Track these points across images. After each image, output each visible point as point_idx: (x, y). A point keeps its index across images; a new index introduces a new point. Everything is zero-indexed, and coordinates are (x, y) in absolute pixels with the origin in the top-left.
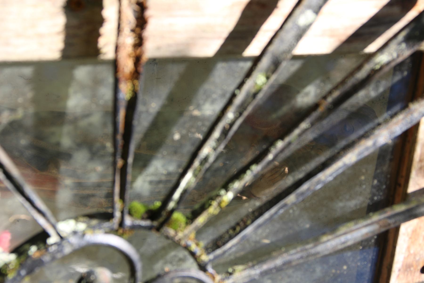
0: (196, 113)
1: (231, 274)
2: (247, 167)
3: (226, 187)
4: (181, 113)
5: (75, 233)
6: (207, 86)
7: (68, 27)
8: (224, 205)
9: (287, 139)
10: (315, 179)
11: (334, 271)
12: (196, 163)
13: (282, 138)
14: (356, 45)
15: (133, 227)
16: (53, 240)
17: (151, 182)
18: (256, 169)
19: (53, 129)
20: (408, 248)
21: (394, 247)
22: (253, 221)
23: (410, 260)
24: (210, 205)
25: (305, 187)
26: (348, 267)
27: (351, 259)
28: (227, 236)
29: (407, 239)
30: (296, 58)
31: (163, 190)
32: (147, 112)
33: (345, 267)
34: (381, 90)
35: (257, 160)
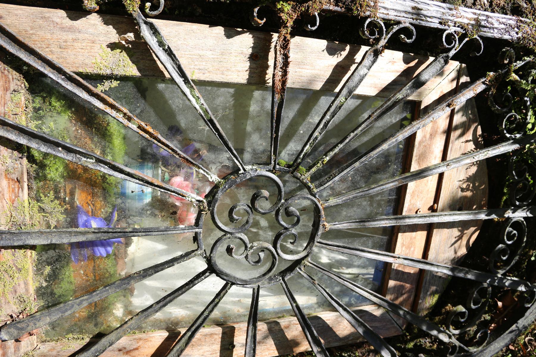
0: (311, 120)
1: (328, 200)
2: (337, 145)
3: (326, 155)
4: (304, 120)
5: (252, 169)
6: (316, 107)
7: (250, 67)
8: (324, 163)
9: (356, 132)
10: (368, 156)
11: (375, 211)
12: (311, 141)
13: (353, 132)
14: (386, 94)
15: (280, 170)
16: (242, 171)
17: (288, 154)
18: (341, 146)
19: (145, 292)
20: (410, 200)
21: (404, 200)
22: (338, 174)
23: (411, 207)
24: (318, 163)
25: (345, 282)
26: (382, 210)
27: (384, 205)
28: (326, 181)
29: (410, 196)
30: (359, 97)
31: (294, 157)
32: (288, 117)
33: (381, 209)
34: (398, 120)
35: (341, 142)
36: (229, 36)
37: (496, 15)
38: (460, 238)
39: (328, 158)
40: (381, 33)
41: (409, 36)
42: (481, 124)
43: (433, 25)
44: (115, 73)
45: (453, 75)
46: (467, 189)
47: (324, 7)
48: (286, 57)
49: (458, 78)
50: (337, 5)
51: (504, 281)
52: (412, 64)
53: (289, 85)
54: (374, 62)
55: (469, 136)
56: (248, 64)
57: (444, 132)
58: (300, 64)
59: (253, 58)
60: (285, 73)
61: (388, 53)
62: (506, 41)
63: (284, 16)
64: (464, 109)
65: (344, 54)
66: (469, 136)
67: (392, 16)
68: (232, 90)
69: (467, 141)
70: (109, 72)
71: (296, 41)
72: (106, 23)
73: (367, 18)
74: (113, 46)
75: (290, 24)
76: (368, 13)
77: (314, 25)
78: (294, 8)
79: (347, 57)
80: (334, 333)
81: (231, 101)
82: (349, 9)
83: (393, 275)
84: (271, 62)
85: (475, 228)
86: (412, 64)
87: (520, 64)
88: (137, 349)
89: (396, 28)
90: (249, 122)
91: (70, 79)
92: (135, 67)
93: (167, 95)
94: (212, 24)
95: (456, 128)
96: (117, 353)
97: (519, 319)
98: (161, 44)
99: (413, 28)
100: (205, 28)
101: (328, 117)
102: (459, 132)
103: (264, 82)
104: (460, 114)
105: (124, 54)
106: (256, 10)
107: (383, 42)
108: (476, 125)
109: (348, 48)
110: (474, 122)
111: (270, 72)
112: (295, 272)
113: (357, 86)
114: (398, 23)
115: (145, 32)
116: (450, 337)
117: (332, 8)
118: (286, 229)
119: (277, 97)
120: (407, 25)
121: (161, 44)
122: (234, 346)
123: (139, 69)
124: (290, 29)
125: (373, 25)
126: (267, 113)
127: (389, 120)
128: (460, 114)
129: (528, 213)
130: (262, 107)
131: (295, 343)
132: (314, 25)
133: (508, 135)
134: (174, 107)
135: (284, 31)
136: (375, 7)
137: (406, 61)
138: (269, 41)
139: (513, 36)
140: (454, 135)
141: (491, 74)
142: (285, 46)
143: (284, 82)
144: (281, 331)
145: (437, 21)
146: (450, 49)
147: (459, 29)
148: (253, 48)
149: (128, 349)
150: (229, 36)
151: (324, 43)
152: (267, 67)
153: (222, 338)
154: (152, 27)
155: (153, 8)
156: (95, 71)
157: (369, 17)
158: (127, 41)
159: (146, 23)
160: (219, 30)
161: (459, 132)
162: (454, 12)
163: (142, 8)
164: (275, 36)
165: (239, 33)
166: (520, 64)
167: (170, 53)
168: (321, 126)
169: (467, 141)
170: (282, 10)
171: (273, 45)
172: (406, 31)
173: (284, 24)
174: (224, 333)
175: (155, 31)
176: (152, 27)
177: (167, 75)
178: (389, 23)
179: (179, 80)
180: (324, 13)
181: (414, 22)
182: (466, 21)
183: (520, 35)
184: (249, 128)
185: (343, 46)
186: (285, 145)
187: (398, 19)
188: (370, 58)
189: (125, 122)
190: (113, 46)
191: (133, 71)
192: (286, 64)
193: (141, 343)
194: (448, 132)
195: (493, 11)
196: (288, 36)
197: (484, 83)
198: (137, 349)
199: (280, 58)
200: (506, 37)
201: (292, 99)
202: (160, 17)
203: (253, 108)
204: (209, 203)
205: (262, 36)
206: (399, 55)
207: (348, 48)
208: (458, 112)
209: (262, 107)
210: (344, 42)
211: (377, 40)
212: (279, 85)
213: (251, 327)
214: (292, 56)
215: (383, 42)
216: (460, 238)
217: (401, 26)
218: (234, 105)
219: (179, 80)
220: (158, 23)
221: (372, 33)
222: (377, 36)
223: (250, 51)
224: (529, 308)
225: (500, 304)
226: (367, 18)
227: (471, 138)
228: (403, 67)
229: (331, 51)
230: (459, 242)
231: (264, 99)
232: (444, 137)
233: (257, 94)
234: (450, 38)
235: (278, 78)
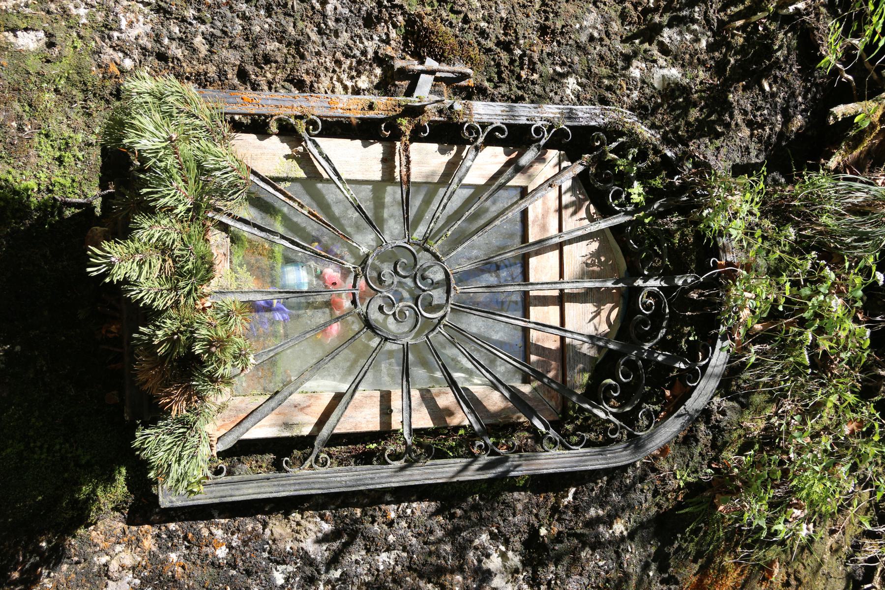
4: (428, 207)
36: (365, 146)
37: (585, 107)
38: (598, 313)
39: (450, 233)
40: (478, 132)
41: (502, 132)
42: (592, 202)
43: (521, 122)
44: (290, 175)
45: (556, 160)
46: (593, 265)
47: (431, 119)
48: (408, 157)
49: (559, 164)
50: (440, 116)
51: (656, 355)
52: (513, 156)
53: (412, 179)
54: (476, 156)
55: (582, 213)
56: (381, 166)
57: (556, 211)
58: (419, 163)
59: (384, 161)
60: (408, 169)
61: (489, 149)
62: (594, 126)
63: (403, 128)
64: (572, 189)
65: (453, 152)
66: (582, 213)
67: (485, 119)
68: (370, 187)
69: (581, 219)
70: (285, 175)
71: (414, 147)
72: (282, 142)
73: (464, 123)
74: (287, 157)
75: (408, 133)
76: (465, 120)
77: (425, 132)
78: (409, 122)
79: (455, 155)
80: (485, 407)
81: (370, 195)
82: (450, 118)
83: (533, 349)
84: (397, 163)
85: (612, 305)
86: (513, 156)
87: (614, 144)
88: (309, 406)
89: (490, 128)
90: (386, 210)
91: (263, 179)
92: (302, 171)
93: (324, 192)
94: (353, 138)
95: (567, 207)
96: (293, 409)
97: (686, 400)
98: (321, 153)
99: (504, 126)
100: (348, 141)
101: (445, 201)
102: (571, 210)
103: (394, 178)
104: (569, 194)
105: (294, 162)
106: (383, 125)
107: (481, 140)
108: (587, 203)
109: (455, 148)
110: (585, 200)
111: (397, 170)
112: (437, 331)
113: (465, 175)
114: (492, 124)
115: (310, 146)
116: (607, 414)
117: (437, 119)
118: (424, 291)
119: (404, 187)
120: (499, 124)
121: (321, 153)
122: (391, 411)
123: (305, 173)
124: (408, 137)
125: (471, 128)
126: (398, 203)
127: (501, 205)
128: (569, 194)
129: (663, 283)
130: (394, 198)
131: (450, 413)
132: (425, 132)
133: (618, 209)
134: (329, 200)
135: (404, 139)
136: (470, 114)
137: (507, 154)
138: (394, 148)
139: (600, 121)
140: (566, 213)
141: (586, 156)
142: (406, 150)
143: (408, 176)
144: (433, 399)
145: (525, 118)
146: (541, 139)
147: (545, 123)
148: (383, 153)
149: (302, 406)
150: (365, 146)
151: (435, 146)
152: (395, 167)
153: (381, 401)
154: (314, 142)
155: (314, 130)
156: (276, 175)
157: (466, 122)
158: (298, 152)
159: (310, 140)
160: (358, 142)
161: (571, 210)
162: (539, 110)
163: (307, 130)
164: (398, 144)
165: (372, 144)
166: (614, 144)
167: (327, 159)
168: (441, 208)
169: (581, 219)
170: (401, 124)
171: (397, 151)
172: (499, 129)
173: (403, 134)
174: (381, 396)
175: (316, 145)
176: (314, 142)
177: (325, 176)
178: (484, 126)
179: (335, 178)
180: (432, 123)
181: (505, 121)
182: (552, 116)
183: (606, 120)
184: (386, 215)
185: (451, 147)
186: (415, 229)
187: (490, 121)
188: (474, 153)
189: (299, 209)
190: (287, 157)
191: (301, 174)
192: (408, 162)
193: (312, 400)
194: (560, 210)
195: (581, 104)
196: (408, 142)
197: (581, 164)
198: (309, 406)
199: (404, 159)
200: (593, 123)
201: (417, 192)
202: (320, 135)
203: (388, 199)
204: (363, 269)
205: (388, 144)
206: (500, 150)
207: (455, 148)
208: (565, 193)
209: (394, 198)
210: (452, 143)
211: (476, 139)
212: (405, 178)
213: (405, 383)
214: (413, 157)
215: (481, 140)
216: (598, 313)
217: (494, 126)
218: (373, 198)
219: (335, 178)
220: (317, 140)
221: (471, 134)
222: (475, 135)
223: (381, 156)
224: (695, 387)
225: (668, 393)
226: (464, 123)
227: (584, 216)
228: (505, 159)
229: (443, 152)
230: (598, 317)
231: (395, 193)
232: (557, 216)
233: (389, 189)
234: (538, 130)
235: (404, 173)
